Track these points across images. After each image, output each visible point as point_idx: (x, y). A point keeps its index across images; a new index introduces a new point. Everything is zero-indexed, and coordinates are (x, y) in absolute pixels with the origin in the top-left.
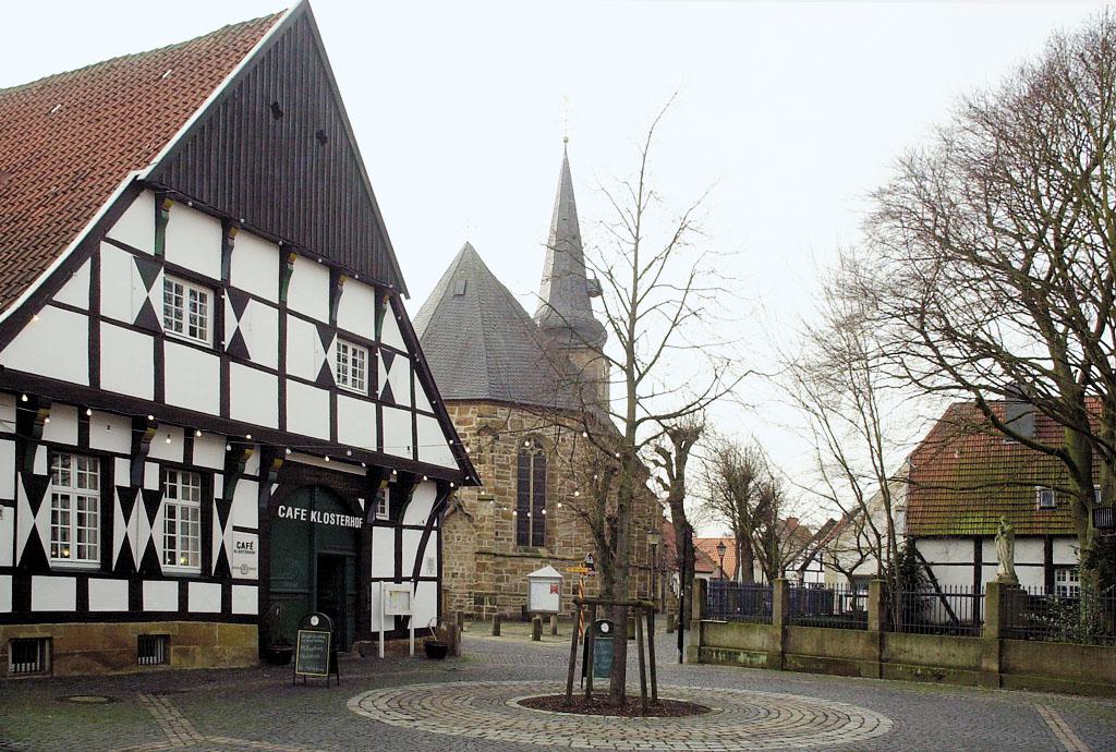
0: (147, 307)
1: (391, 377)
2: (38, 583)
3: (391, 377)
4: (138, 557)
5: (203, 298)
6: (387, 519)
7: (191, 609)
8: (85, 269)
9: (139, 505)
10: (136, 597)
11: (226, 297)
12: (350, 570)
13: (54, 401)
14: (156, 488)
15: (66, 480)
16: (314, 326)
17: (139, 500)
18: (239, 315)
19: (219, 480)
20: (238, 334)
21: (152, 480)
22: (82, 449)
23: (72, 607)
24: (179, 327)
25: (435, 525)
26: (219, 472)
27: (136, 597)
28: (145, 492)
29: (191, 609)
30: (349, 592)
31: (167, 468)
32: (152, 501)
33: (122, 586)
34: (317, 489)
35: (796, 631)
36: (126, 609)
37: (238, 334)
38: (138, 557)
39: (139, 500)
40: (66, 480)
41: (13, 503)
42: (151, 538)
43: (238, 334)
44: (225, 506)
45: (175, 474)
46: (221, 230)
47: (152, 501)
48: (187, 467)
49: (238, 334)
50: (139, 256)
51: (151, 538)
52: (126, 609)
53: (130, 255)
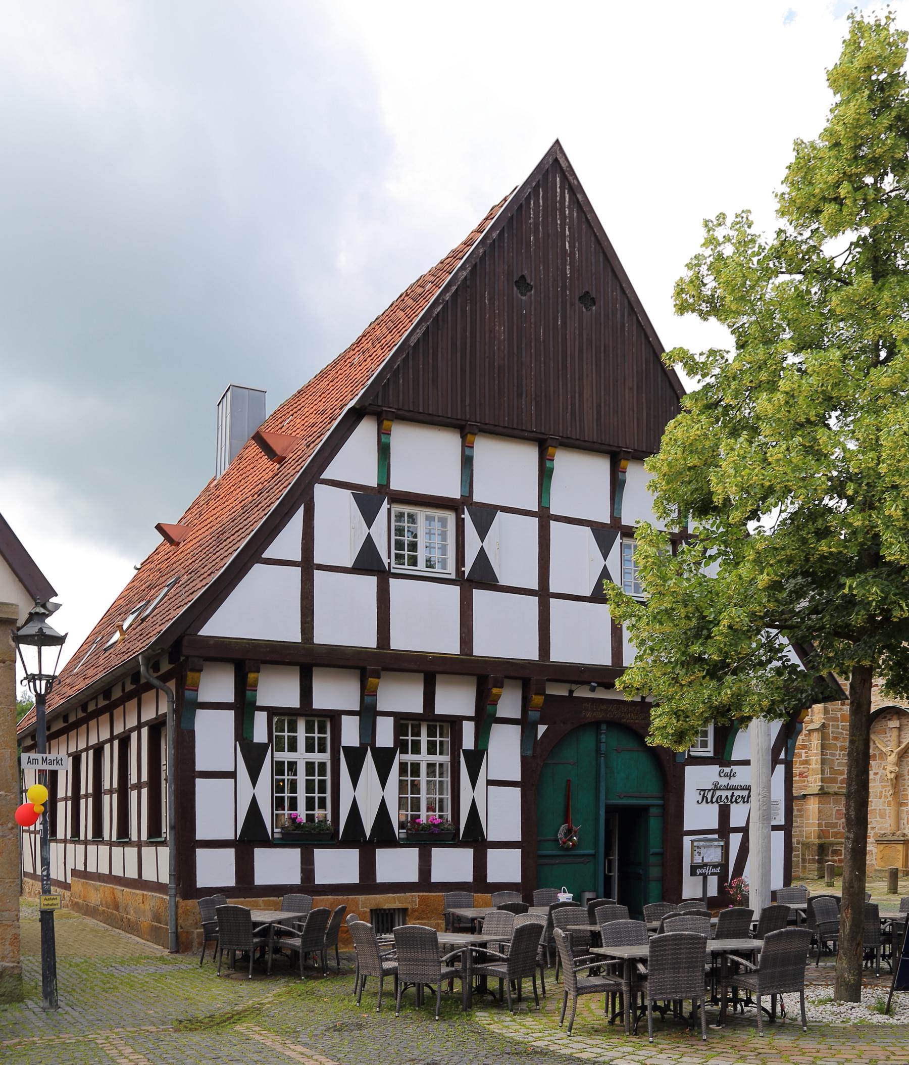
0: (369, 544)
1: (490, 545)
2: (261, 856)
3: (490, 545)
4: (368, 822)
5: (443, 521)
6: (711, 754)
7: (436, 878)
8: (297, 519)
9: (369, 765)
10: (368, 866)
11: (466, 516)
12: (654, 824)
13: (549, 680)
14: (390, 743)
15: (416, 750)
16: (588, 530)
17: (369, 763)
18: (482, 533)
19: (468, 729)
20: (482, 555)
21: (385, 735)
22: (306, 709)
23: (414, 877)
24: (413, 561)
25: (782, 756)
26: (469, 718)
27: (368, 866)
28: (463, 750)
29: (436, 878)
30: (652, 851)
31: (403, 721)
32: (384, 760)
33: (352, 856)
34: (604, 727)
35: (902, 996)
36: (356, 880)
37: (482, 555)
38: (368, 822)
39: (369, 763)
40: (416, 750)
41: (232, 775)
42: (383, 801)
43: (482, 555)
44: (475, 759)
45: (419, 726)
46: (460, 440)
47: (384, 760)
48: (429, 717)
49: (482, 555)
50: (597, 528)
51: (383, 801)
52: (356, 880)
53: (348, 493)
